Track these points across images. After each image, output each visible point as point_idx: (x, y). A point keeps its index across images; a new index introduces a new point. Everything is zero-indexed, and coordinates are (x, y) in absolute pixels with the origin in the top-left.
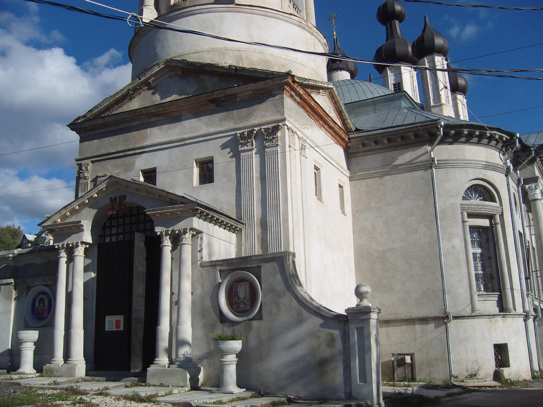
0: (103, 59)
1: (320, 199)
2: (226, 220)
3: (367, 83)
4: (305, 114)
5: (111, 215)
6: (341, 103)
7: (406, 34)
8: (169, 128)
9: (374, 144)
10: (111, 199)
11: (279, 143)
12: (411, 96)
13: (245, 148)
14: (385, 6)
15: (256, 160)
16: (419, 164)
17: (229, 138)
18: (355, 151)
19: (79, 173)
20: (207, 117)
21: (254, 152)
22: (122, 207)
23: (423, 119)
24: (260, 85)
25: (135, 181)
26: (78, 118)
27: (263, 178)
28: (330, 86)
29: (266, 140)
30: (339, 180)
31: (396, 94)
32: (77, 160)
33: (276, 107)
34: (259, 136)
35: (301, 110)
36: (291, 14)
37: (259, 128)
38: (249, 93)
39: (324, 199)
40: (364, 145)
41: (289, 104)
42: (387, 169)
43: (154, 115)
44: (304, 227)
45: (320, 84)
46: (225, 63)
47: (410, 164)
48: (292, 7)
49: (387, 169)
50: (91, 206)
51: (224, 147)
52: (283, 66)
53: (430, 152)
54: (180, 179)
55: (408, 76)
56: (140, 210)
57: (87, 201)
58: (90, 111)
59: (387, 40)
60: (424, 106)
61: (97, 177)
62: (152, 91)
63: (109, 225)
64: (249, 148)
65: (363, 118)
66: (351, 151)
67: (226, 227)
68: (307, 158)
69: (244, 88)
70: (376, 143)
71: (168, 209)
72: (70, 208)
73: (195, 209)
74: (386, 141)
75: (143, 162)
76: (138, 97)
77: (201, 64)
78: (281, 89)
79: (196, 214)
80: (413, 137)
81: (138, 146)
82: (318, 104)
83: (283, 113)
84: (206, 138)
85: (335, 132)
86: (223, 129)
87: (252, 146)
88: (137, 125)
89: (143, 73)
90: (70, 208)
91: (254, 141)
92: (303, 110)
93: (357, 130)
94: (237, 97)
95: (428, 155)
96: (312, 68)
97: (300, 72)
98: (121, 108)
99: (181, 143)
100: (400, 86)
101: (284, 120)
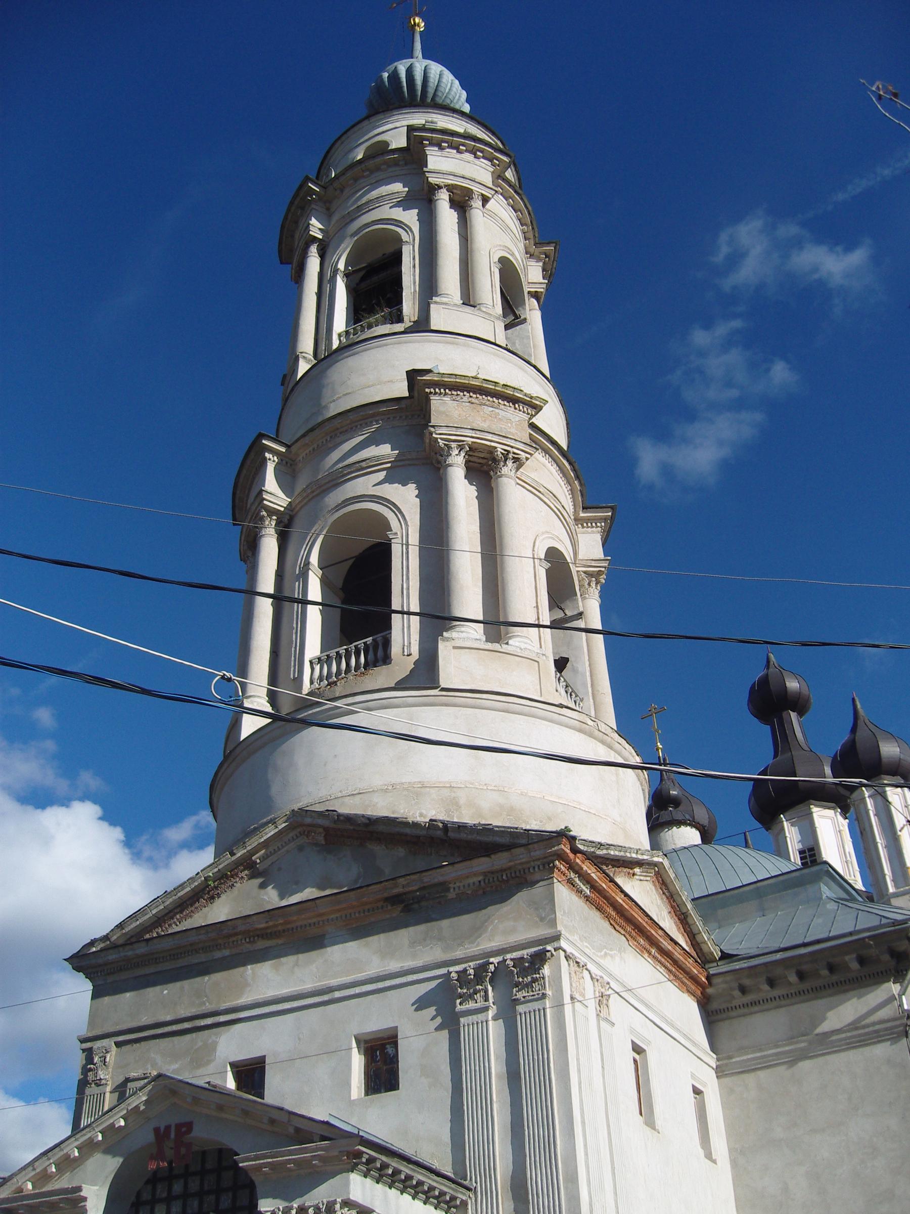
0: (177, 834)
1: (650, 1123)
2: (429, 1181)
3: (741, 852)
4: (606, 924)
5: (155, 1173)
6: (685, 897)
7: (815, 738)
8: (296, 964)
9: (766, 987)
10: (157, 1130)
11: (549, 992)
12: (841, 872)
13: (471, 1005)
14: (764, 682)
15: (495, 1031)
16: (877, 1027)
17: (433, 984)
18: (724, 1006)
19: (85, 1071)
20: (382, 936)
21: (491, 1013)
22: (183, 1151)
23: (875, 921)
24: (500, 860)
25: (215, 1086)
26: (92, 943)
27: (513, 1076)
28: (656, 859)
29: (517, 985)
30: (693, 1076)
31: (806, 871)
32: (83, 1041)
33: (536, 909)
34: (501, 975)
35: (595, 915)
36: (561, 706)
37: (500, 958)
38: (476, 879)
39: (659, 1123)
40: (743, 990)
41: (566, 899)
42: (803, 1045)
43: (264, 935)
44: (616, 1194)
45: (634, 855)
46: (421, 815)
47: (857, 1029)
48: (563, 691)
49: (803, 1045)
50: (109, 1149)
51: (421, 1004)
52: (550, 819)
53: (900, 996)
54: (322, 1085)
55: (830, 829)
56: (224, 1159)
57: (100, 1138)
58: (120, 926)
59: (776, 756)
60: (875, 894)
61: (128, 1080)
62: (258, 881)
63: (150, 1197)
64: (479, 1005)
65: (737, 929)
66: (714, 1006)
67: (428, 1198)
68: (613, 1024)
69: (462, 869)
70: (771, 983)
71: (292, 1154)
72: (58, 1154)
73: (356, 1152)
74: (793, 978)
75: (233, 1045)
76: (229, 892)
77: (369, 819)
78: (547, 867)
79: (356, 1164)
80: (855, 965)
81: (224, 1006)
82: (633, 901)
83: (553, 923)
84: (381, 985)
85: (675, 962)
86: (419, 963)
87: (486, 1000)
88: (224, 958)
89: (240, 841)
90: (58, 1154)
91: (490, 988)
92: (598, 913)
93: (725, 956)
94: (448, 890)
95: (896, 1003)
96: (607, 806)
97: (590, 830)
98: (189, 920)
99: (324, 997)
100: (814, 855)
101: (557, 937)
